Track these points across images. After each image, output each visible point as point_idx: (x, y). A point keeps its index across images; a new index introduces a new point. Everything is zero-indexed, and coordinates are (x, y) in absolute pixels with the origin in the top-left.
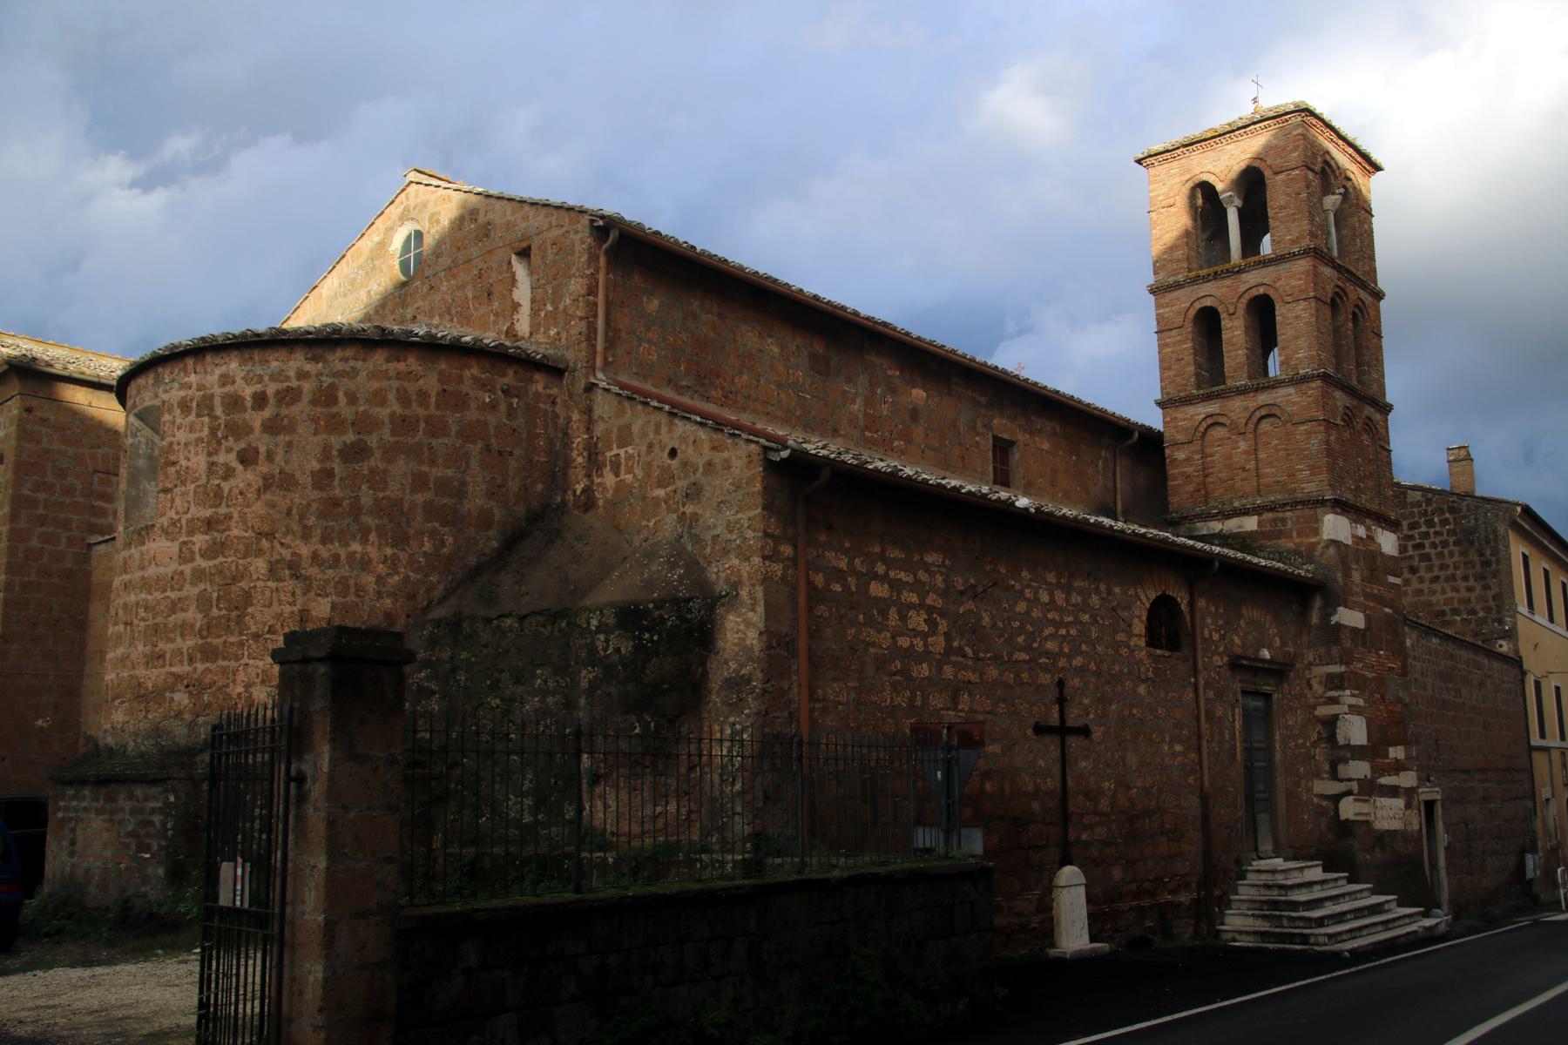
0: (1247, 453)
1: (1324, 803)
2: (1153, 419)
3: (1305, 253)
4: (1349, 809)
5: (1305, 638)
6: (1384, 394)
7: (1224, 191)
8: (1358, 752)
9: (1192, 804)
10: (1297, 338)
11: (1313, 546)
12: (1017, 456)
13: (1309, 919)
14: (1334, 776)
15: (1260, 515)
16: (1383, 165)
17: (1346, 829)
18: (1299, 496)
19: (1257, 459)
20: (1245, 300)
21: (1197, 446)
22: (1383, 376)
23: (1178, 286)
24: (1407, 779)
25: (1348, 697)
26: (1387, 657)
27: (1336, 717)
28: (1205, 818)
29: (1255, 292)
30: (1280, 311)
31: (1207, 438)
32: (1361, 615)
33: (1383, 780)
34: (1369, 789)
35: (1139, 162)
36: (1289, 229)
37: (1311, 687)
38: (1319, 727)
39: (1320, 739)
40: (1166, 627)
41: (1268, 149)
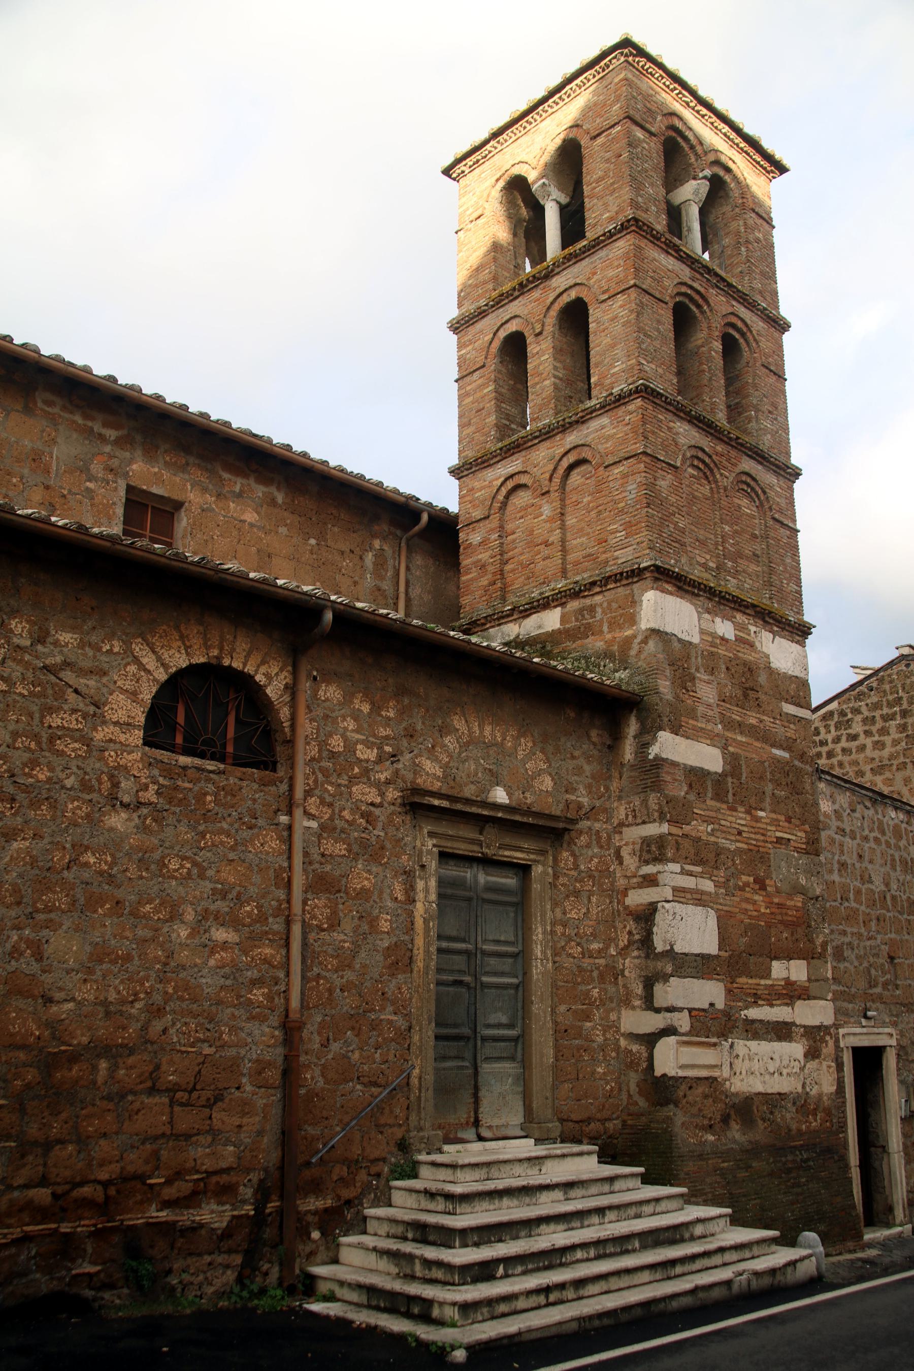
0: (550, 520)
1: (635, 1048)
2: (445, 495)
3: (624, 228)
4: (670, 1058)
5: (615, 785)
6: (788, 454)
7: (535, 182)
8: (699, 966)
9: (260, 1041)
10: (613, 346)
11: (627, 642)
12: (184, 522)
13: (448, 1267)
14: (649, 1004)
15: (563, 605)
16: (786, 162)
17: (662, 1090)
18: (611, 569)
19: (563, 527)
20: (554, 313)
21: (494, 522)
22: (786, 430)
23: (481, 314)
24: (815, 1013)
25: (672, 874)
26: (775, 823)
27: (652, 909)
28: (290, 1072)
29: (566, 299)
30: (594, 314)
31: (510, 508)
32: (716, 753)
33: (753, 1013)
34: (713, 1026)
35: (447, 172)
36: (606, 205)
37: (620, 859)
38: (631, 925)
39: (630, 943)
40: (211, 720)
41: (588, 110)
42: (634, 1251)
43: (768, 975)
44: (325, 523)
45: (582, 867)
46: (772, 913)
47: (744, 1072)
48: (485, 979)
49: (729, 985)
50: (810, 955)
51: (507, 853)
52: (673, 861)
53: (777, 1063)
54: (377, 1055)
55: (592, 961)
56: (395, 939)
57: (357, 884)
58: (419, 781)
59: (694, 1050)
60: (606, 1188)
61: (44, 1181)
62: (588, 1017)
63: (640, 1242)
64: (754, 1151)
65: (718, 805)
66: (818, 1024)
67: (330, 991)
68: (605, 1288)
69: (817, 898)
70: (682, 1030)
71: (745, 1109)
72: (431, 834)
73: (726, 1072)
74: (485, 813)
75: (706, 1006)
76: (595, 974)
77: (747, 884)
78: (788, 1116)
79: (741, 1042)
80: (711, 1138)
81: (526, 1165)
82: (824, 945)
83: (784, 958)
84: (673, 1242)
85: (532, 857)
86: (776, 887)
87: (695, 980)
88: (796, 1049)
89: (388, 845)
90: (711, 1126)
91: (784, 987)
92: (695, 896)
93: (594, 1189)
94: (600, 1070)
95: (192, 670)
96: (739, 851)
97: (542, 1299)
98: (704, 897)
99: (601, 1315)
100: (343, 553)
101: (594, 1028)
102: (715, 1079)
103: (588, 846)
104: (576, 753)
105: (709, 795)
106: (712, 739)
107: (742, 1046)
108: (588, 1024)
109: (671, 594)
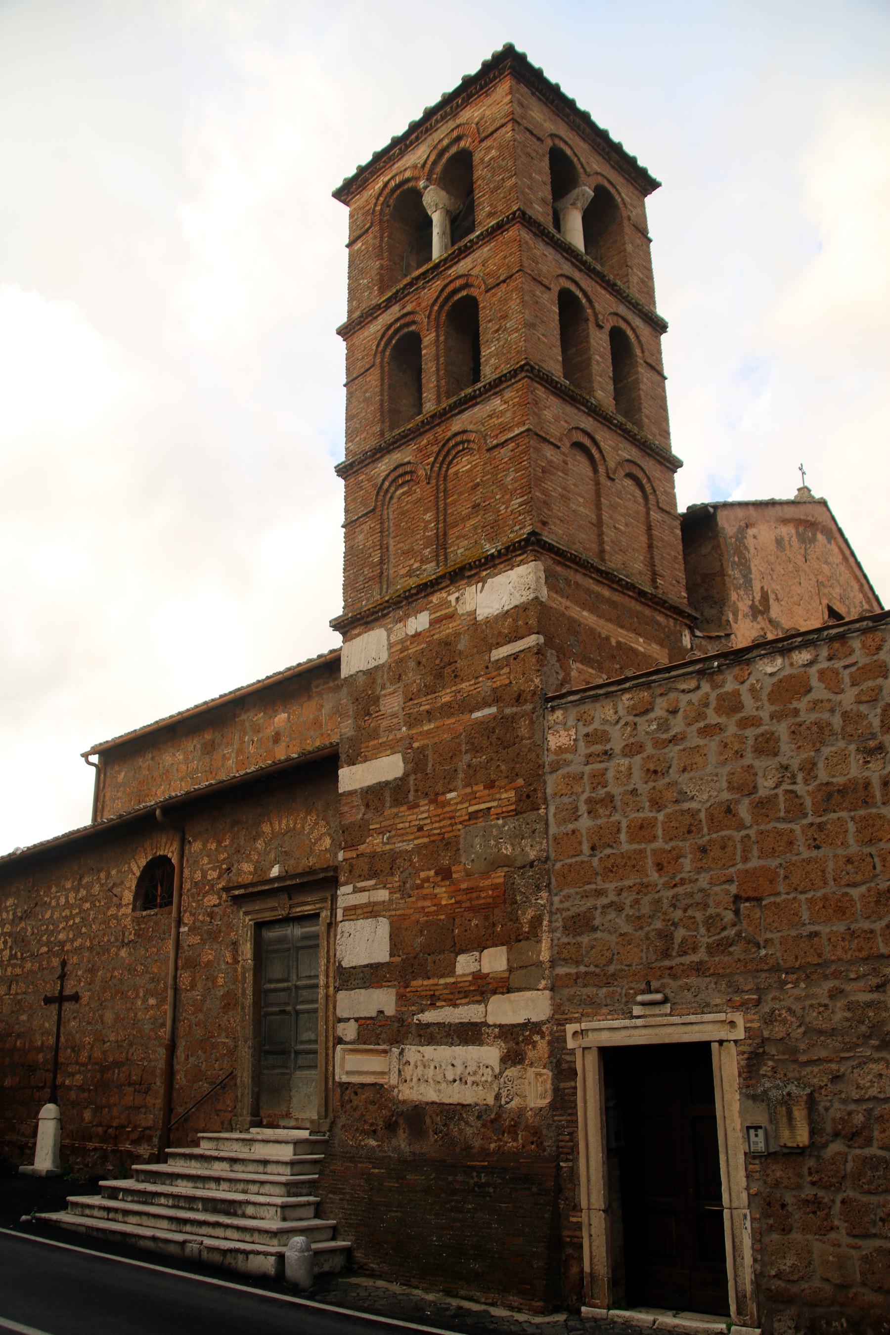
24: (528, 1006)
28: (170, 1073)
33: (429, 1016)
34: (379, 1033)
42: (198, 1210)
43: (452, 973)
46: (456, 902)
47: (415, 1080)
48: (299, 1007)
49: (402, 990)
50: (514, 937)
51: (298, 909)
52: (346, 883)
53: (459, 1069)
54: (216, 1065)
56: (226, 989)
57: (205, 959)
58: (240, 880)
59: (359, 1057)
60: (261, 1168)
61: (100, 1125)
63: (203, 1206)
64: (415, 1163)
67: (190, 1027)
68: (139, 1222)
69: (531, 865)
70: (347, 1039)
71: (416, 1117)
72: (246, 913)
73: (394, 1080)
74: (267, 888)
75: (374, 1014)
77: (427, 880)
78: (469, 1131)
79: (414, 1048)
80: (373, 1143)
81: (241, 1144)
82: (536, 922)
83: (474, 949)
84: (227, 1213)
85: (318, 906)
86: (465, 869)
87: (363, 991)
88: (490, 1054)
89: (223, 929)
90: (375, 1131)
91: (471, 983)
92: (365, 910)
93: (251, 1168)
95: (149, 864)
96: (419, 848)
97: (105, 1214)
98: (376, 908)
99: (99, 1230)
102: (382, 1085)
107: (412, 1052)
109: (359, 635)
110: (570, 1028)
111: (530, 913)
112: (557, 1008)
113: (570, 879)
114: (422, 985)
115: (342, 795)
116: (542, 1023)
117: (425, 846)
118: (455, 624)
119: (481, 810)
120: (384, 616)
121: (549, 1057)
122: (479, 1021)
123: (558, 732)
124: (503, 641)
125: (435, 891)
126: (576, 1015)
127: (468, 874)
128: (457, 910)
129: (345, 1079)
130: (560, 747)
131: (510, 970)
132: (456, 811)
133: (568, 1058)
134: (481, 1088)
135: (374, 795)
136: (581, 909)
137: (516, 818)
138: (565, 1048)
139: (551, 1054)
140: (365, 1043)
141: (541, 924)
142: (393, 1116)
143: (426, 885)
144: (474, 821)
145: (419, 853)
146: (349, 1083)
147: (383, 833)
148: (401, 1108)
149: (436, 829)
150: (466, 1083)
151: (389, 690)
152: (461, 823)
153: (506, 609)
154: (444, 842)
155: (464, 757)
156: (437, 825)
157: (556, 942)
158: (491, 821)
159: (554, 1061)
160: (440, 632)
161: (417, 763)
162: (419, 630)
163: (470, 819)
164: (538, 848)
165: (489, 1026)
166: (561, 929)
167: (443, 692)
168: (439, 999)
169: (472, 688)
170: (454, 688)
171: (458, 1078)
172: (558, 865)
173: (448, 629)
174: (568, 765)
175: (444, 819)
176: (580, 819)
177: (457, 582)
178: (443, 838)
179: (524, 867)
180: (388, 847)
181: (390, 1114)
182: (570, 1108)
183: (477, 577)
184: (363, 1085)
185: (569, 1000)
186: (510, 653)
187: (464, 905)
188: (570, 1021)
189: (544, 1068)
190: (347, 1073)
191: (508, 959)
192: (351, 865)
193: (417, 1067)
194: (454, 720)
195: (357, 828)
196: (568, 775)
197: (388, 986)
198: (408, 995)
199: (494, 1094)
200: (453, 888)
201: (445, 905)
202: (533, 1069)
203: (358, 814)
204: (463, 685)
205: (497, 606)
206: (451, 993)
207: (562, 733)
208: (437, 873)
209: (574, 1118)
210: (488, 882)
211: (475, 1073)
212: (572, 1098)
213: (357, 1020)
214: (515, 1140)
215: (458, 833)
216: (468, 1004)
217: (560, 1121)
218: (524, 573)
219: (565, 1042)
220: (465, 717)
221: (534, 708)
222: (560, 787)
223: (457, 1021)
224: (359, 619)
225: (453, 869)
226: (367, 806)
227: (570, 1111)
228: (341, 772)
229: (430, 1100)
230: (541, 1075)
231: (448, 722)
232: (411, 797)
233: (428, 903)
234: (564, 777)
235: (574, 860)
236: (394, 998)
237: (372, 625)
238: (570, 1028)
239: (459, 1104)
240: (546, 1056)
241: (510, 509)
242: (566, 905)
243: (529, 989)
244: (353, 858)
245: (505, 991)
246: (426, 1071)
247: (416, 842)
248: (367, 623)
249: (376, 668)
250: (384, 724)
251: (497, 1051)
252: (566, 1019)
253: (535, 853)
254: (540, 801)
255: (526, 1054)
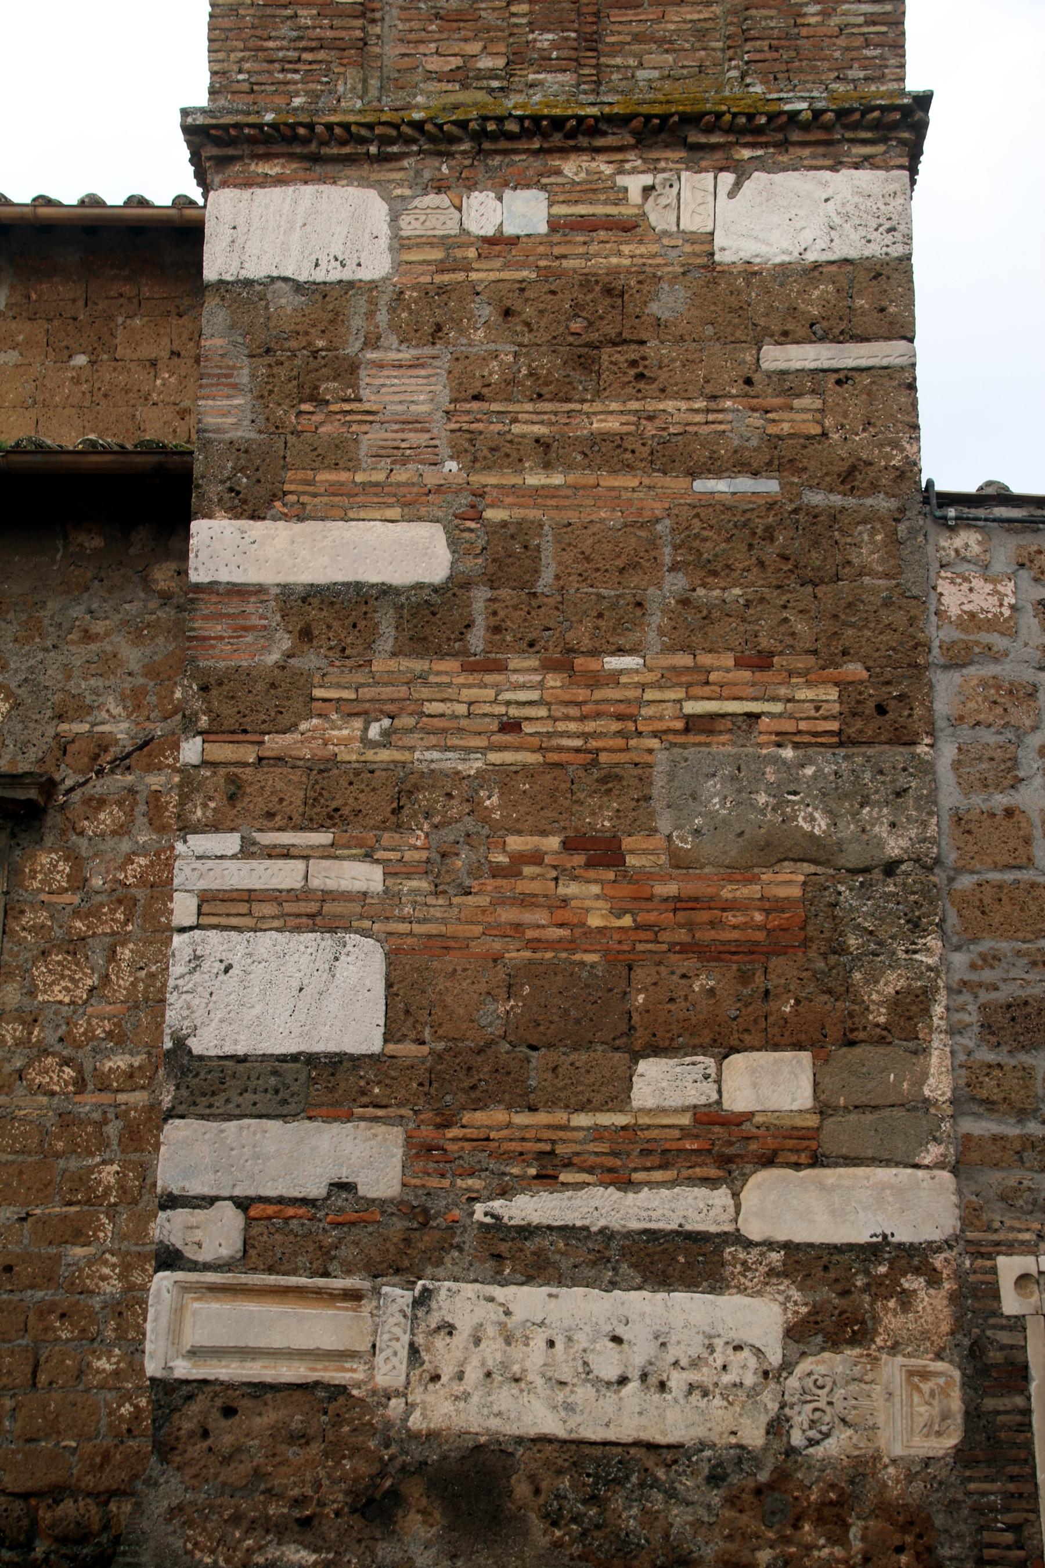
33: (528, 1208)
44: (111, 318)
45: (97, 882)
46: (638, 927)
50: (827, 1033)
53: (640, 1353)
55: (106, 1098)
62: (78, 1235)
65: (418, 665)
66: (862, 1236)
69: (890, 868)
73: (390, 1370)
75: (316, 1190)
76: (112, 1130)
79: (469, 1290)
88: (756, 1317)
94: (103, 1364)
96: (504, 777)
100: (153, 363)
101: (97, 1259)
102: (341, 1390)
103: (121, 831)
104: (99, 627)
105: (386, 643)
106: (412, 505)
108: (79, 1251)
109: (280, 181)
110: (1009, 1267)
111: (892, 982)
112: (970, 1214)
113: (997, 918)
114: (509, 1125)
115: (198, 588)
116: (934, 1248)
117: (526, 771)
118: (642, 250)
119: (723, 716)
120: (383, 158)
121: (952, 1333)
122: (713, 1229)
123: (966, 580)
124: (802, 332)
125: (562, 890)
126: (1027, 1236)
127: (679, 862)
128: (640, 947)
129: (183, 1369)
130: (972, 615)
131: (823, 1108)
132: (640, 703)
133: (1004, 1338)
134: (718, 1402)
135: (333, 615)
136: (1029, 991)
137: (842, 752)
138: (997, 1313)
139: (958, 1326)
140: (271, 1270)
141: (926, 1012)
142: (382, 1474)
143: (528, 870)
144: (702, 738)
145: (505, 789)
146: (205, 1382)
147: (368, 718)
148: (416, 1452)
149: (569, 735)
150: (662, 1386)
151: (393, 355)
152: (655, 734)
153: (811, 257)
154: (596, 774)
155: (669, 578)
156: (573, 727)
157: (962, 1057)
158: (760, 745)
159: (966, 1342)
160: (587, 256)
161: (500, 558)
162: (509, 230)
163: (687, 730)
164: (913, 833)
165: (749, 1244)
166: (976, 1029)
167: (598, 406)
168: (565, 1166)
169: (699, 418)
170: (634, 405)
171: (634, 1374)
172: (966, 882)
173: (617, 257)
174: (996, 660)
175: (598, 715)
176: (1022, 788)
177: (650, 147)
178: (595, 763)
179: (866, 870)
180: (385, 755)
181: (374, 1469)
182: (1015, 1461)
183: (718, 155)
184: (260, 1390)
185: (1003, 1198)
186: (826, 365)
187: (664, 936)
188: (1010, 1248)
189: (938, 1357)
190: (194, 1353)
191: (816, 1084)
192: (233, 780)
193: (477, 1341)
194: (635, 483)
195: (260, 686)
196: (996, 682)
197: (375, 1119)
198: (451, 1147)
199: (764, 1420)
200: (625, 890)
201: (601, 930)
202: (900, 1359)
203: (266, 649)
204: (669, 405)
205: (786, 245)
206: (614, 1154)
207: (977, 583)
208: (568, 846)
209: (1027, 1488)
210: (752, 891)
211: (695, 1363)
212: (1021, 1438)
213: (243, 1204)
214: (842, 1540)
215: (649, 758)
216: (672, 1184)
217: (984, 1494)
218: (876, 189)
219: (996, 1296)
220: (675, 483)
221: (902, 510)
222: (972, 705)
223: (635, 1225)
224: (294, 139)
225: (627, 843)
226: (306, 635)
227: (1014, 1470)
228: (196, 526)
229: (532, 1432)
230: (925, 1375)
231: (609, 481)
232: (477, 639)
233: (541, 917)
234: (984, 683)
235: (1009, 876)
236: (399, 1153)
237: (329, 169)
238: (1009, 1267)
239: (637, 1444)
240: (945, 1328)
241: (835, 21)
242: (987, 975)
243: (887, 1163)
244: (246, 765)
245: (804, 1159)
246: (517, 1351)
247: (494, 757)
248: (315, 159)
249: (348, 286)
250: (373, 437)
251: (776, 1308)
252: (998, 1244)
253: (904, 843)
254: (920, 727)
255: (876, 1320)
